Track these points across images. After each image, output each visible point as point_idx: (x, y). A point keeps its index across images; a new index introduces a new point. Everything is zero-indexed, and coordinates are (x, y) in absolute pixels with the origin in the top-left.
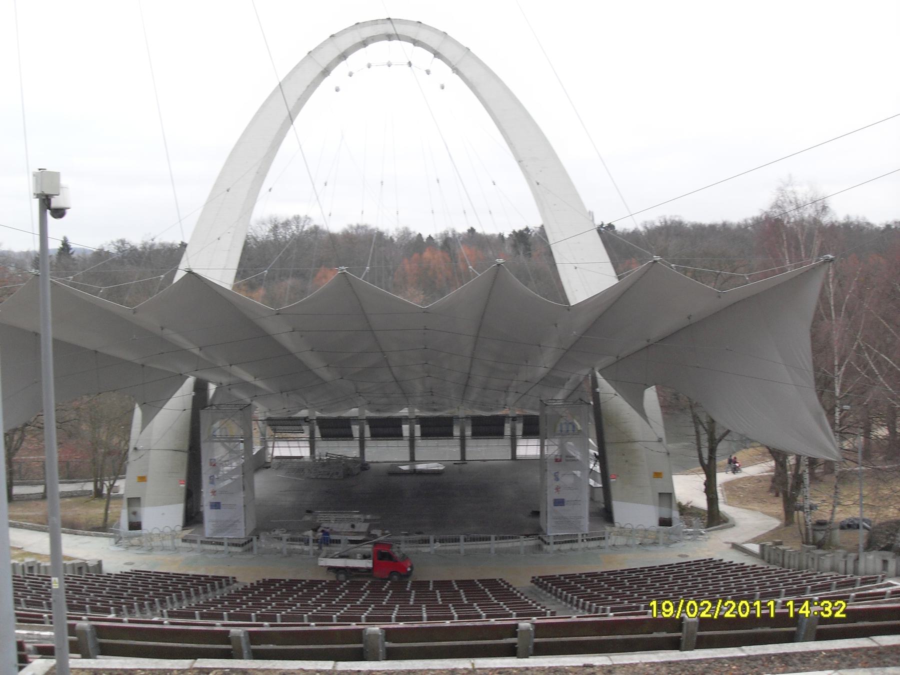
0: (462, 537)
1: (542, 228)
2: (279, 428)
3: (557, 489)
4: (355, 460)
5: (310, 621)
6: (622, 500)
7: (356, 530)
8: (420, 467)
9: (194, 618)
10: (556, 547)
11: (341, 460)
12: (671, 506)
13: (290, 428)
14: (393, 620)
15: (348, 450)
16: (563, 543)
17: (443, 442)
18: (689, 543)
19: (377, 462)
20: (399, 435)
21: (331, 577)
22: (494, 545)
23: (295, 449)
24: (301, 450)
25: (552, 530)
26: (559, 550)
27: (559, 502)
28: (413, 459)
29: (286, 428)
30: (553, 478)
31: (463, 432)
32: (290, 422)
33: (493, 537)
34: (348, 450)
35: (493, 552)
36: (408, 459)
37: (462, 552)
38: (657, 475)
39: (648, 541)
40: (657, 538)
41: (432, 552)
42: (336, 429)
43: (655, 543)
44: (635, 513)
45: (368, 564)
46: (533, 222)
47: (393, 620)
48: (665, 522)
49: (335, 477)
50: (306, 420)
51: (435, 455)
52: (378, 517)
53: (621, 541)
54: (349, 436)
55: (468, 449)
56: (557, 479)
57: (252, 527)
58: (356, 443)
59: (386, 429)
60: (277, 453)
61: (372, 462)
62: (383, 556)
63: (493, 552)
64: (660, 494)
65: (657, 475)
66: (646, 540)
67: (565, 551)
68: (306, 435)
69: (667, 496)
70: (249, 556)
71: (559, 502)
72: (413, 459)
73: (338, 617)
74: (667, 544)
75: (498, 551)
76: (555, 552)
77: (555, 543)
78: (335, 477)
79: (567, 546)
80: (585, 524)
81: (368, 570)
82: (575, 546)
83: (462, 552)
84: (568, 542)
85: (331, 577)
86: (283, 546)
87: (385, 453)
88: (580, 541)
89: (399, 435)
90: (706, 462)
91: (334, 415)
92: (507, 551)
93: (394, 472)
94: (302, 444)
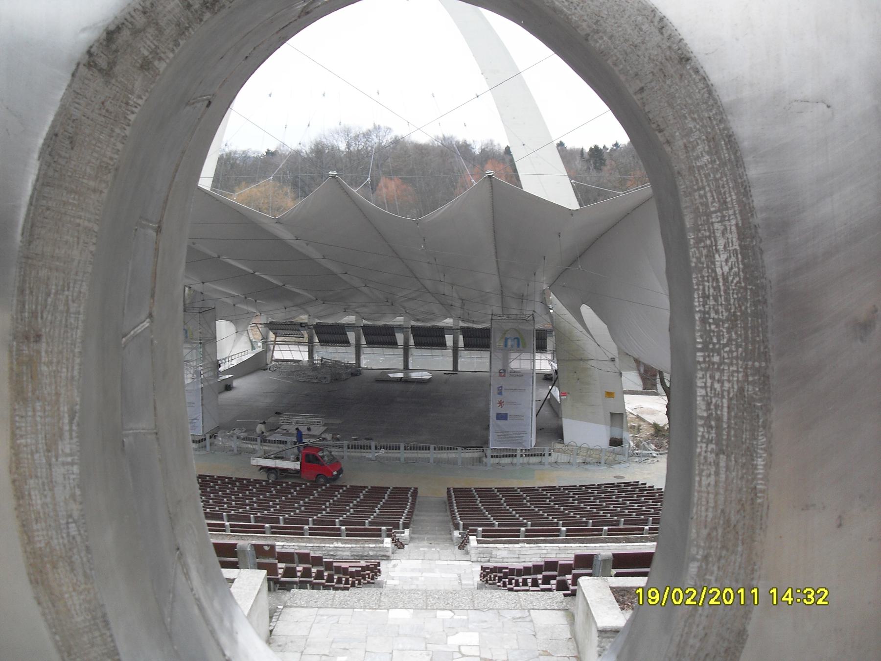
0: (402, 446)
1: (508, 150)
2: (281, 332)
3: (501, 403)
4: (347, 366)
5: (341, 525)
6: (571, 417)
7: (310, 433)
8: (414, 375)
9: (222, 519)
10: (526, 460)
11: (336, 364)
12: (622, 428)
13: (291, 332)
14: (401, 526)
15: (344, 355)
16: (503, 456)
17: (437, 352)
18: (634, 465)
19: (372, 369)
20: (442, 345)
21: (263, 476)
22: (432, 455)
23: (291, 352)
24: (300, 354)
25: (494, 443)
26: (528, 464)
27: (502, 417)
28: (406, 367)
29: (286, 332)
30: (496, 391)
31: (456, 342)
32: (283, 327)
33: (432, 447)
34: (344, 355)
35: (432, 461)
36: (402, 368)
37: (402, 460)
38: (610, 395)
39: (592, 459)
40: (599, 458)
41: (374, 458)
42: (333, 335)
43: (598, 463)
44: (584, 432)
45: (296, 466)
46: (501, 142)
47: (401, 526)
48: (616, 442)
49: (323, 381)
50: (302, 325)
51: (428, 364)
52: (338, 422)
53: (563, 458)
54: (346, 342)
55: (460, 361)
56: (500, 393)
57: (211, 425)
58: (352, 350)
59: (381, 337)
60: (277, 355)
61: (367, 369)
62: (309, 458)
63: (432, 461)
64: (611, 414)
65: (610, 395)
66: (589, 459)
67: (504, 466)
68: (306, 340)
69: (618, 417)
70: (203, 452)
71: (502, 417)
72: (406, 367)
73: (341, 521)
74: (609, 464)
75: (438, 462)
76: (492, 465)
77: (492, 457)
78: (323, 381)
79: (507, 460)
80: (532, 440)
81: (297, 471)
82: (515, 460)
83: (402, 460)
84: (509, 456)
85: (263, 476)
86: (234, 444)
87: (377, 360)
88: (518, 456)
89: (442, 345)
90: (668, 385)
91: (380, 323)
92: (449, 461)
93: (382, 379)
94: (302, 348)
